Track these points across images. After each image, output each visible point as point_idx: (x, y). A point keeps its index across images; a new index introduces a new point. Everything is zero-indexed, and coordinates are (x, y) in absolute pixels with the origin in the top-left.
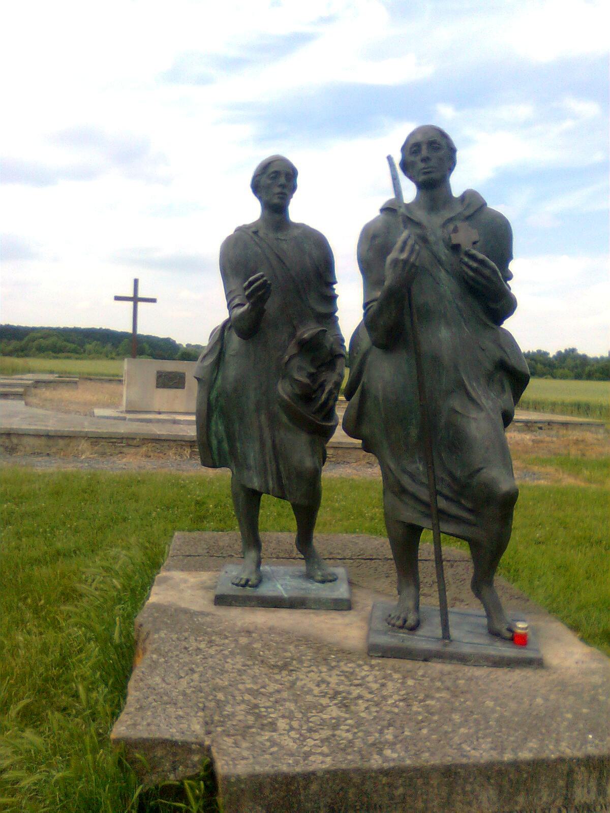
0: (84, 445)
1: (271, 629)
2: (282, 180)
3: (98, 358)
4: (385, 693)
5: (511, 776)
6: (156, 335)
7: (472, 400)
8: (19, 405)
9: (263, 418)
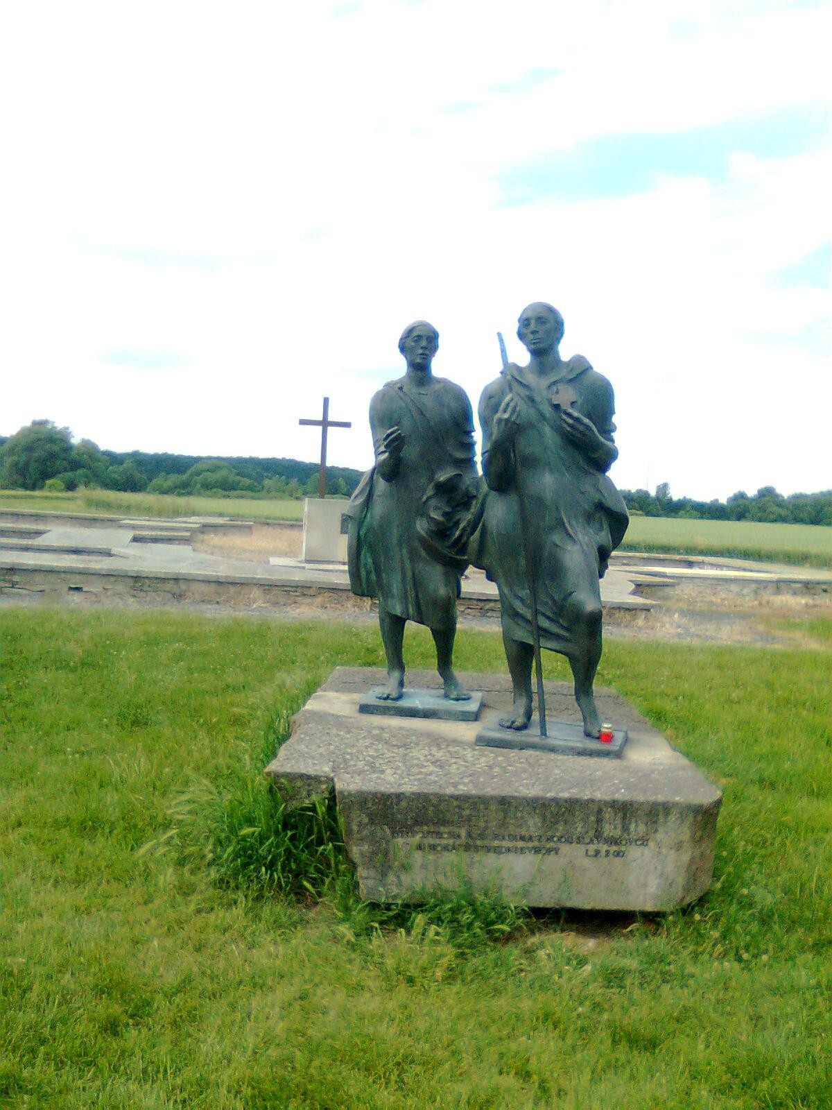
0: (256, 593)
1: (401, 728)
2: (424, 343)
3: (281, 498)
5: (553, 809)
6: (356, 469)
7: (568, 534)
8: (185, 550)
9: (404, 551)
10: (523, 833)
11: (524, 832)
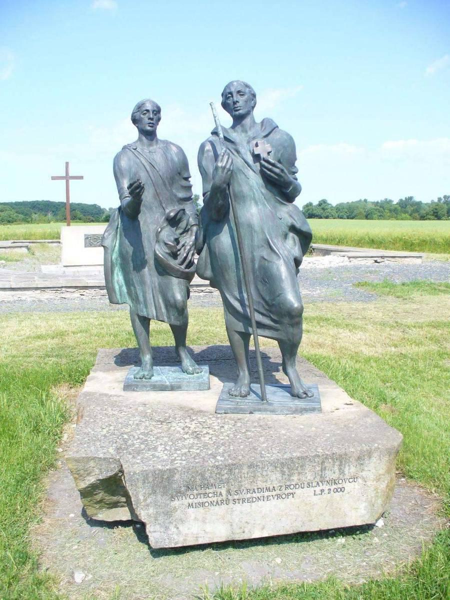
4: (223, 430)
10: (268, 486)
11: (269, 485)
